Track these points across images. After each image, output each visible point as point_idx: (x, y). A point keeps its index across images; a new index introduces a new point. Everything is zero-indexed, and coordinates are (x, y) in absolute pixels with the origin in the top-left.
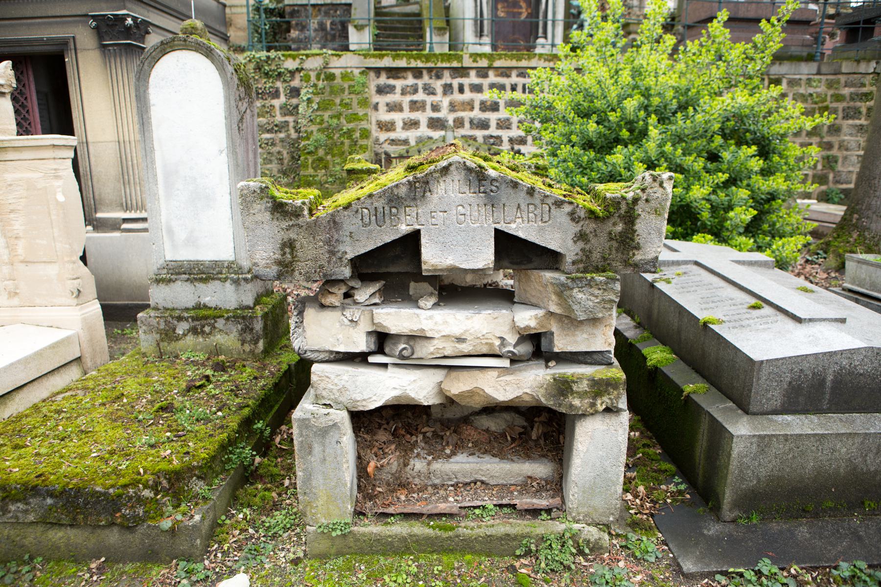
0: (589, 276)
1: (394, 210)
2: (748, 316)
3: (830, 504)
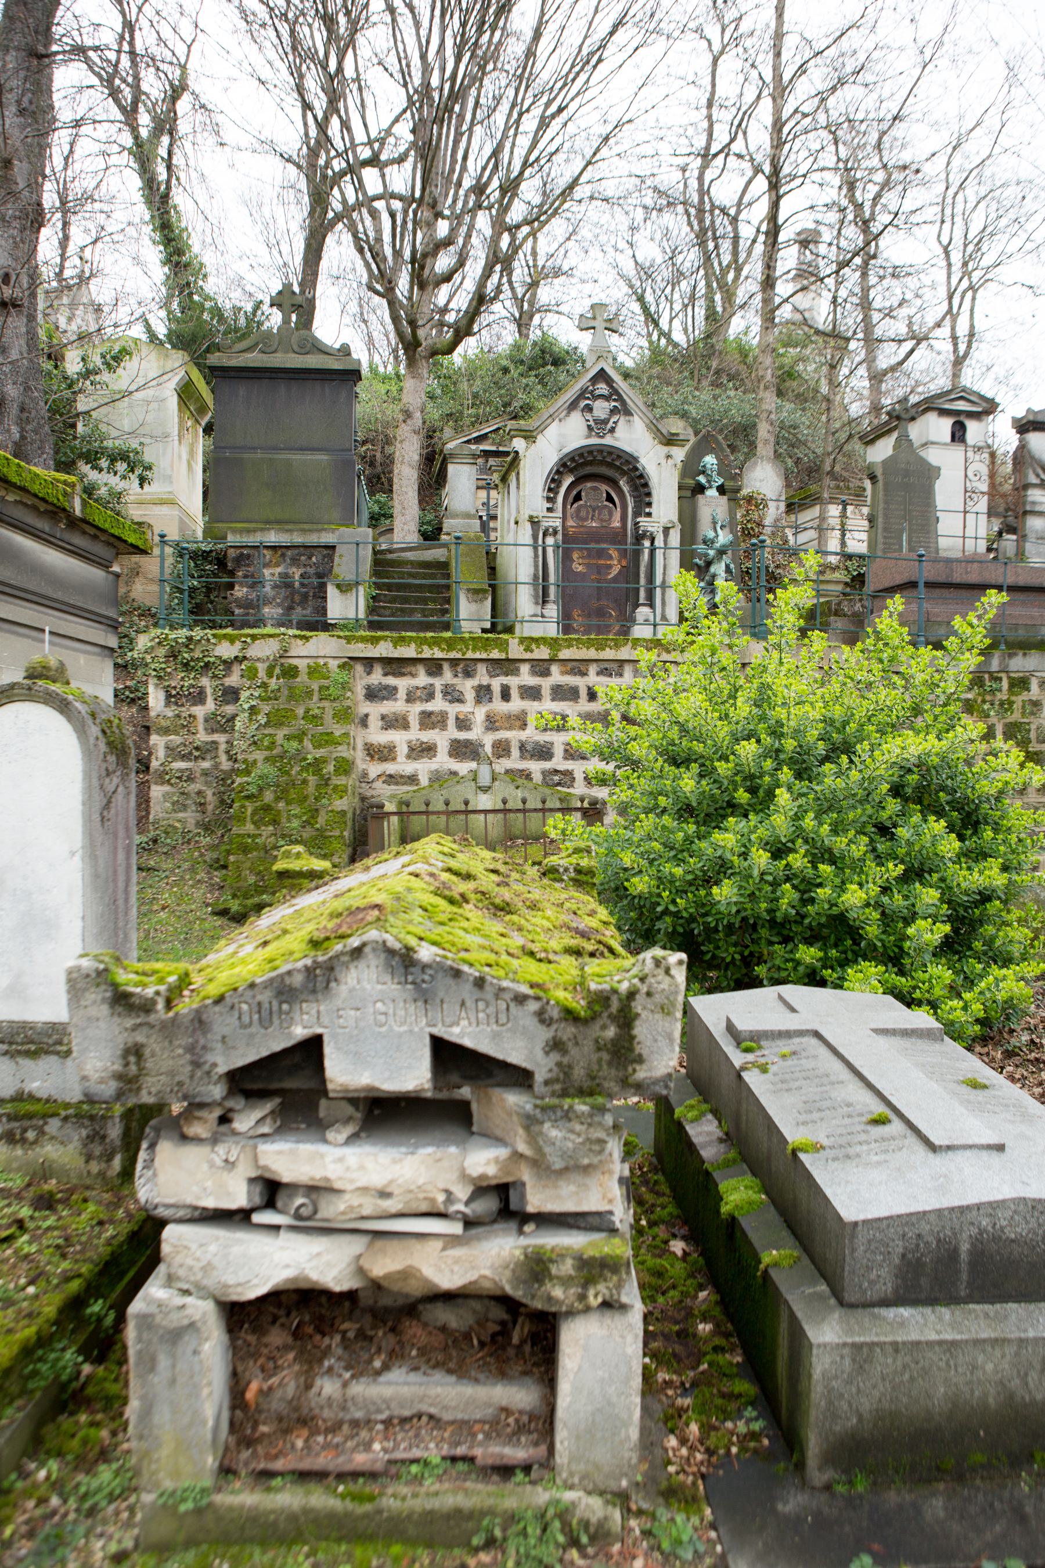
0: (567, 1102)
1: (285, 1007)
2: (863, 1137)
3: (979, 1458)
